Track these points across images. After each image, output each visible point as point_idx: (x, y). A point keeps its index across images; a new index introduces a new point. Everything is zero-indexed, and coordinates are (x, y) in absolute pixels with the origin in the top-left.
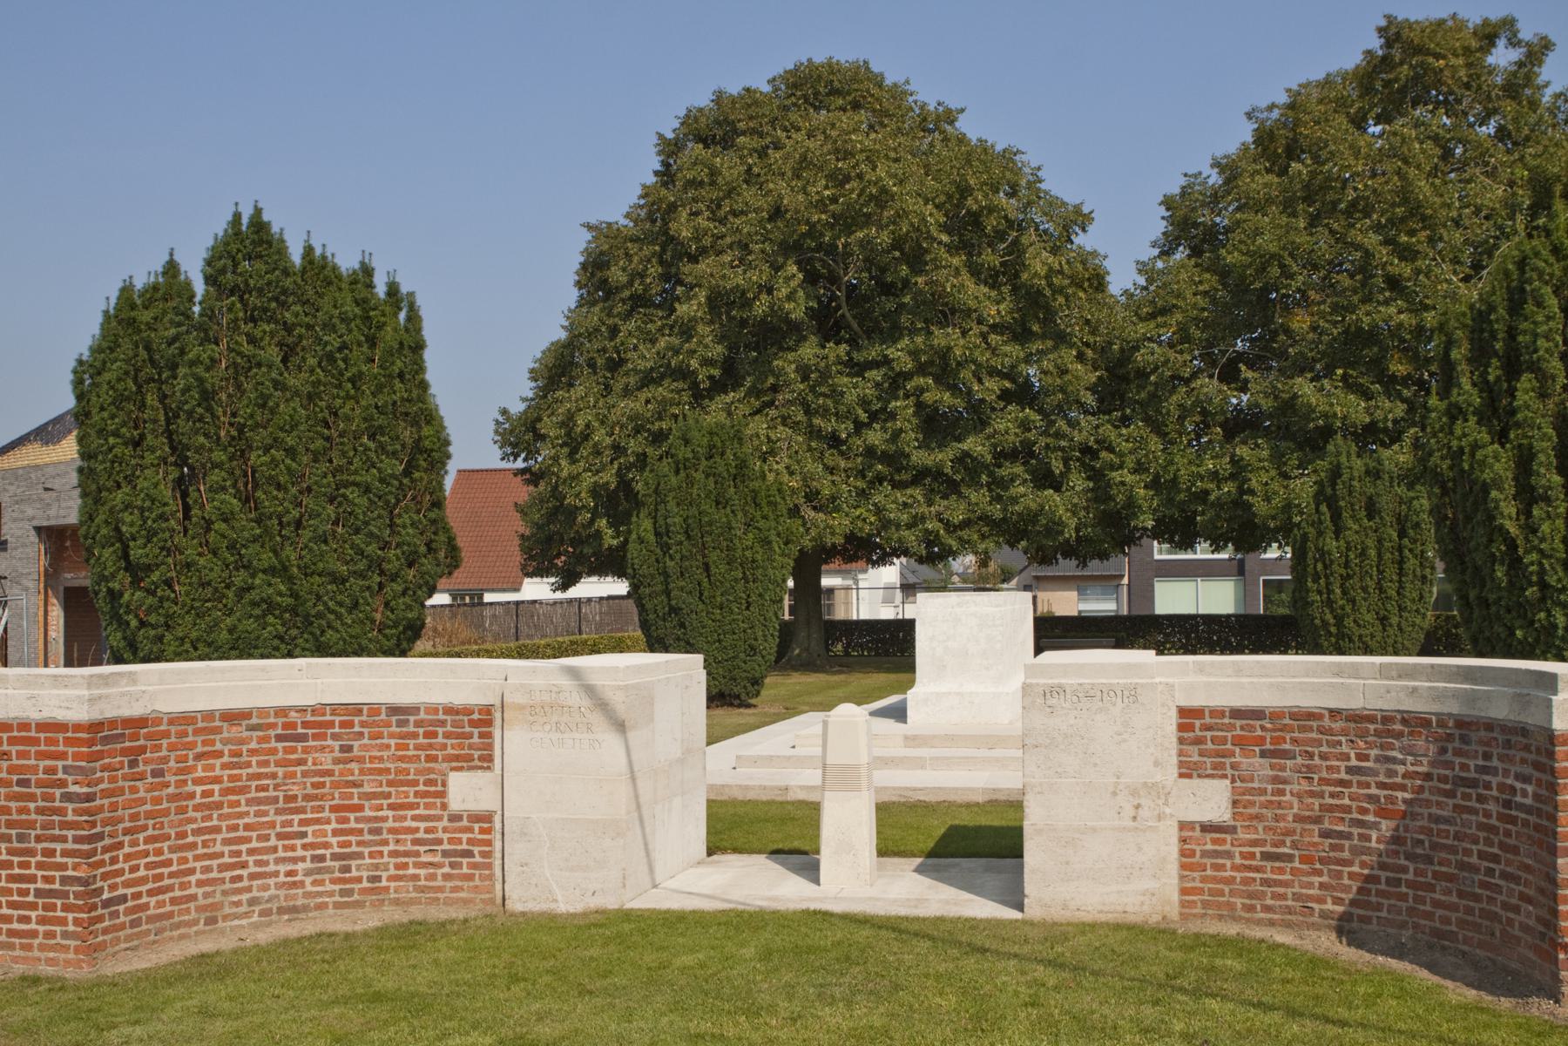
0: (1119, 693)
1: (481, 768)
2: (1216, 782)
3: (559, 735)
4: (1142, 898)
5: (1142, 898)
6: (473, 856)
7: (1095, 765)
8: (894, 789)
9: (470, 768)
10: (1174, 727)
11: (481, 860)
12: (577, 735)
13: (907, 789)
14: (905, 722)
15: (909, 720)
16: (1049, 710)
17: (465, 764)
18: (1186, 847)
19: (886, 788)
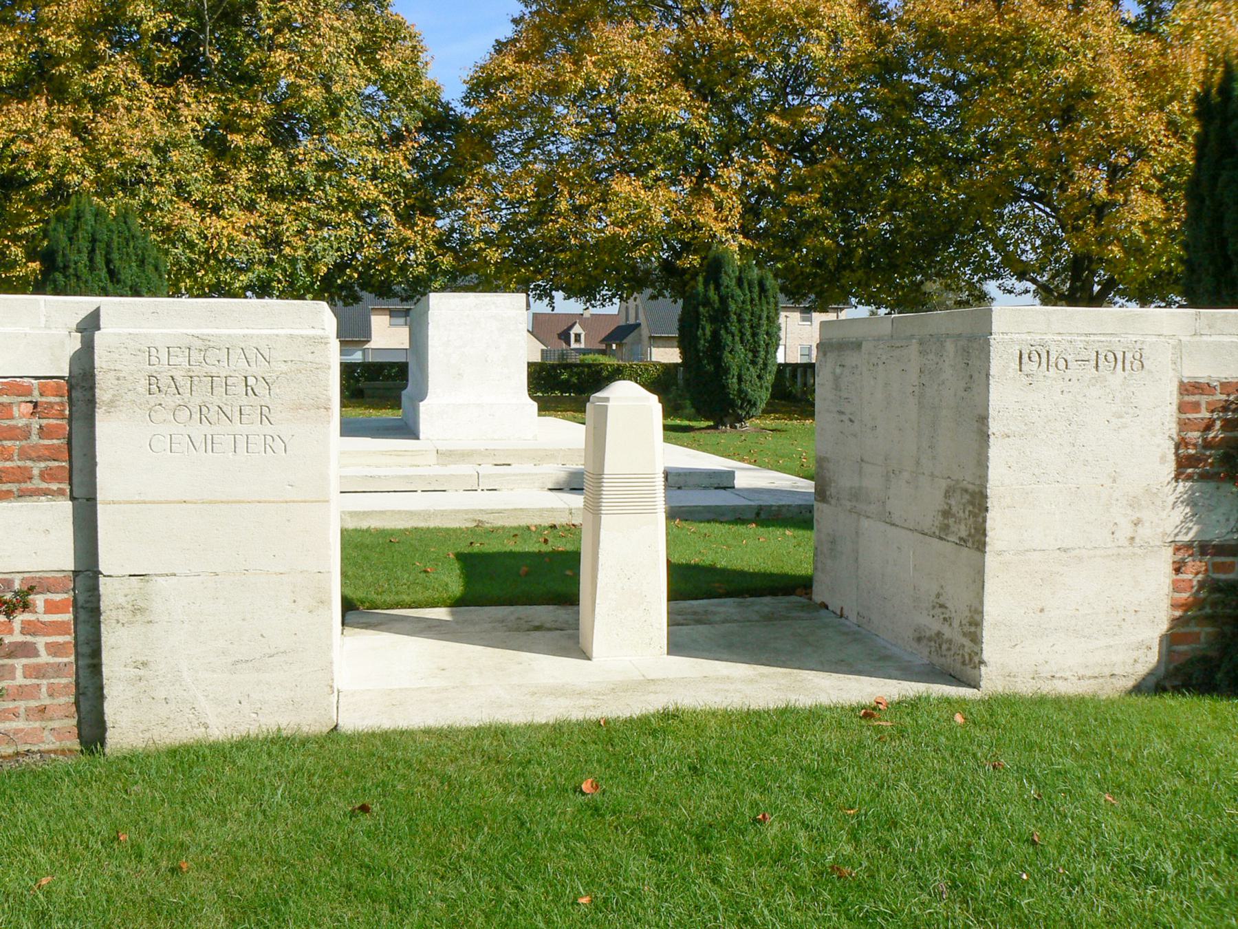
0: (1120, 357)
1: (46, 493)
2: (44, 503)
3: (206, 428)
4: (1136, 654)
5: (1136, 654)
6: (36, 654)
7: (1086, 463)
8: (467, 512)
9: (22, 495)
10: (1175, 407)
11: (52, 660)
12: (237, 427)
13: (475, 511)
14: (417, 438)
15: (421, 436)
16: (1025, 380)
17: (14, 487)
18: (1181, 576)
19: (458, 511)
